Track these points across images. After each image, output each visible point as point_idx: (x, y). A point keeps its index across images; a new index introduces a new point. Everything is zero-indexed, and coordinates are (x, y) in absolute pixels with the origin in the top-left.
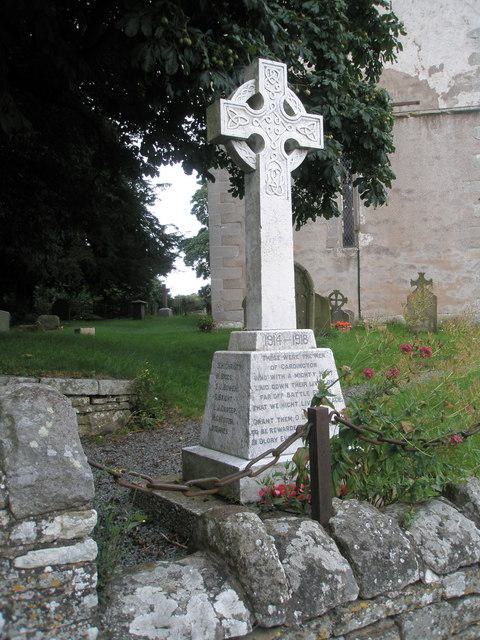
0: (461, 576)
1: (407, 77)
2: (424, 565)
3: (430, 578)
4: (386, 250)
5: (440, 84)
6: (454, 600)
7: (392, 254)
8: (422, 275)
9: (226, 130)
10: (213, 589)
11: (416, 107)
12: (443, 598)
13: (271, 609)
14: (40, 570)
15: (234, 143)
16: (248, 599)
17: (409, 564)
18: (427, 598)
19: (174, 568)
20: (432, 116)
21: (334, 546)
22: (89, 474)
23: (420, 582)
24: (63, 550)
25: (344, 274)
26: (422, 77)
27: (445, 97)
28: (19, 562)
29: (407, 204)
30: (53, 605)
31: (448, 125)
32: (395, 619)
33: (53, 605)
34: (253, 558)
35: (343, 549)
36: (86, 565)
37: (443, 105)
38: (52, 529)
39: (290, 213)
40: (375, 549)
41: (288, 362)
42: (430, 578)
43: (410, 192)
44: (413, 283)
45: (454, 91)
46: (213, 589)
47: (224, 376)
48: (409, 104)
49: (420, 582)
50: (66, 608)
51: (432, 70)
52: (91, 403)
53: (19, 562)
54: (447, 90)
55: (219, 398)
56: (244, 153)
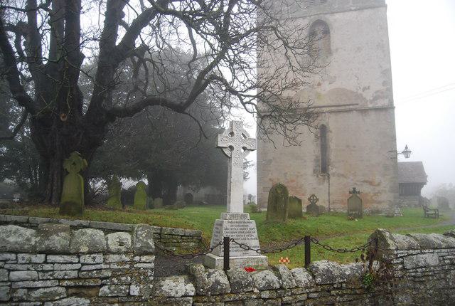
0: (268, 292)
1: (352, 92)
2: (255, 287)
3: (256, 290)
4: (343, 175)
5: (368, 95)
6: (265, 299)
7: (345, 177)
8: (354, 189)
9: (220, 145)
10: (186, 282)
11: (357, 106)
12: (260, 298)
13: (202, 290)
14: (140, 268)
15: (224, 150)
16: (196, 287)
17: (249, 285)
18: (254, 296)
19: (177, 277)
20: (364, 111)
21: (226, 277)
22: (154, 247)
23: (252, 291)
24: (145, 264)
25: (321, 186)
26: (360, 91)
27: (371, 102)
28: (135, 266)
29: (353, 152)
30: (142, 277)
31: (373, 115)
32: (243, 301)
33: (142, 277)
34: (199, 276)
35: (229, 279)
36: (151, 269)
37: (370, 106)
38: (144, 259)
39: (396, 111)
40: (238, 279)
41: (237, 224)
42: (256, 290)
43: (354, 147)
44: (350, 193)
45: (375, 98)
46: (186, 282)
47: (217, 228)
48: (353, 105)
49: (252, 291)
50: (145, 278)
51: (364, 89)
52: (181, 238)
53: (135, 266)
54: (371, 98)
55: (216, 236)
56: (227, 152)
